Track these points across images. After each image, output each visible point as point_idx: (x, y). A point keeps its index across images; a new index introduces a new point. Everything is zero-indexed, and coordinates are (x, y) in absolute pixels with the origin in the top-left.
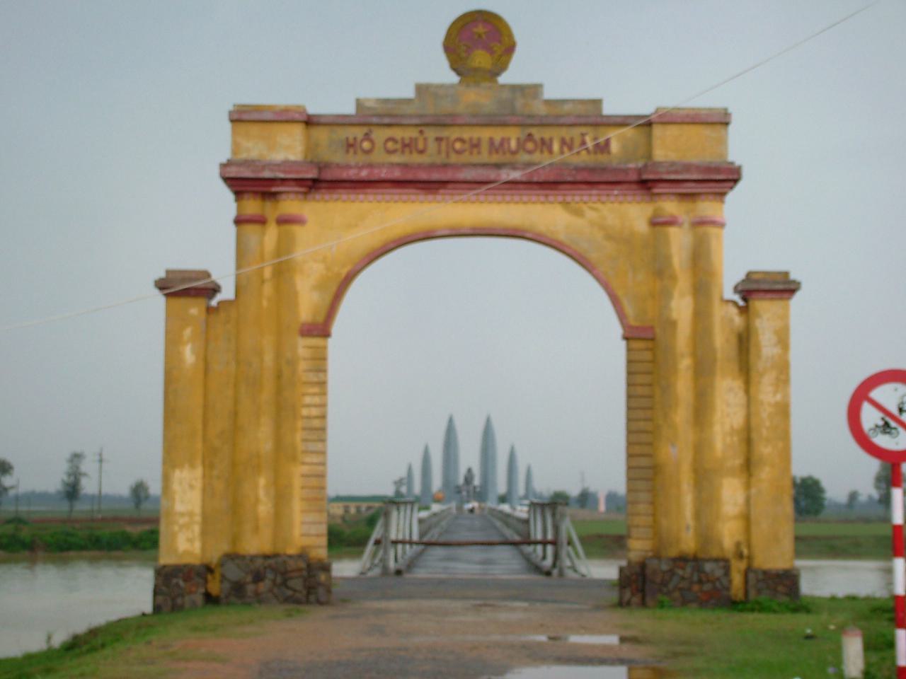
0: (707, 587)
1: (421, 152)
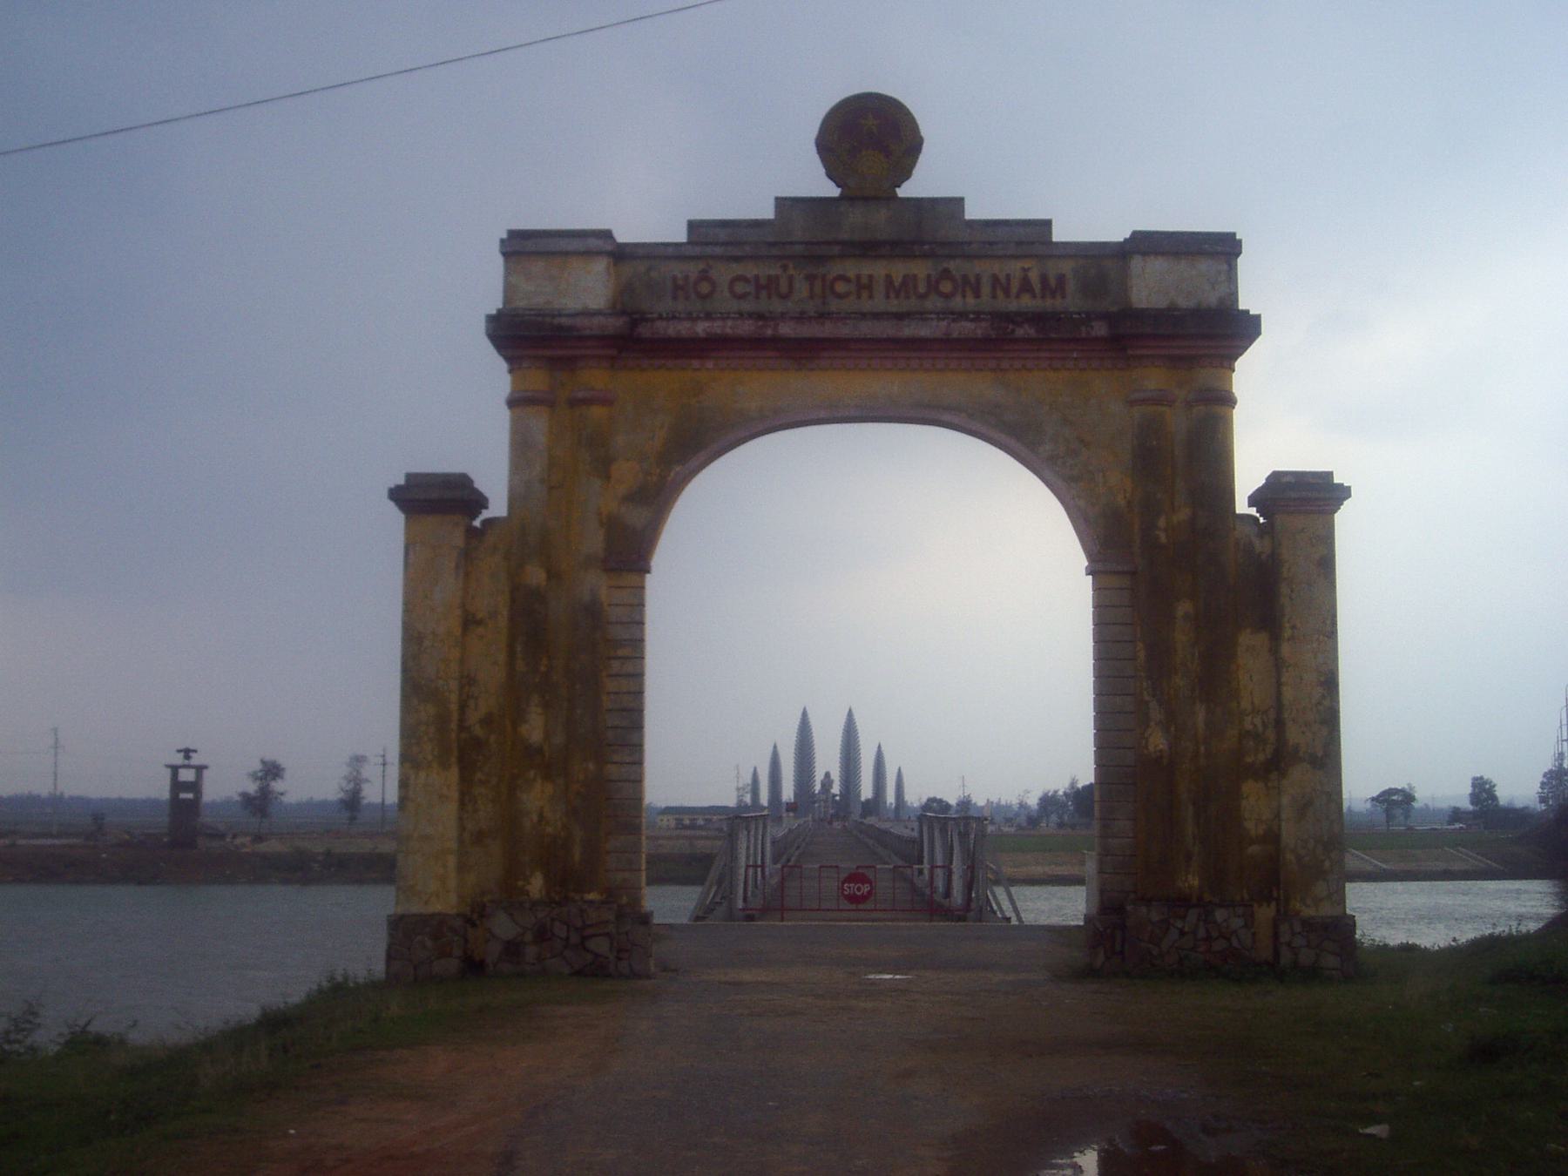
0: (1219, 945)
1: (784, 297)
